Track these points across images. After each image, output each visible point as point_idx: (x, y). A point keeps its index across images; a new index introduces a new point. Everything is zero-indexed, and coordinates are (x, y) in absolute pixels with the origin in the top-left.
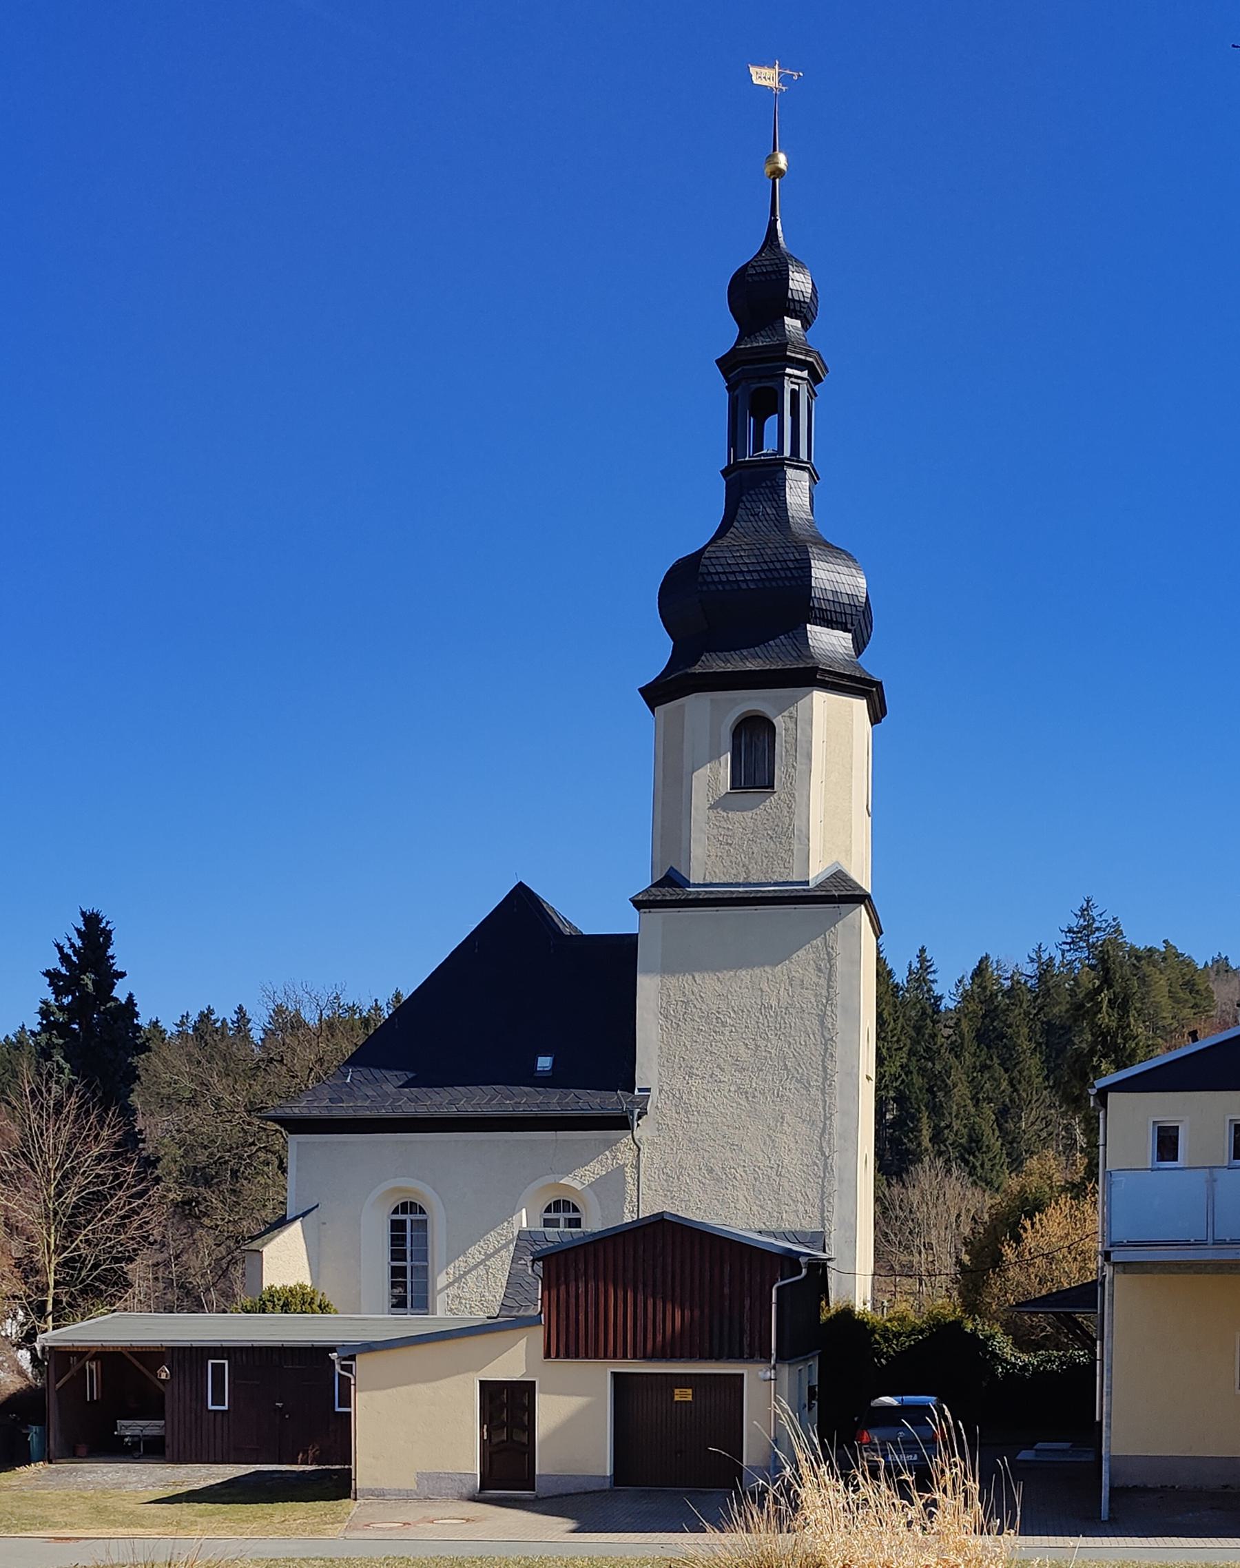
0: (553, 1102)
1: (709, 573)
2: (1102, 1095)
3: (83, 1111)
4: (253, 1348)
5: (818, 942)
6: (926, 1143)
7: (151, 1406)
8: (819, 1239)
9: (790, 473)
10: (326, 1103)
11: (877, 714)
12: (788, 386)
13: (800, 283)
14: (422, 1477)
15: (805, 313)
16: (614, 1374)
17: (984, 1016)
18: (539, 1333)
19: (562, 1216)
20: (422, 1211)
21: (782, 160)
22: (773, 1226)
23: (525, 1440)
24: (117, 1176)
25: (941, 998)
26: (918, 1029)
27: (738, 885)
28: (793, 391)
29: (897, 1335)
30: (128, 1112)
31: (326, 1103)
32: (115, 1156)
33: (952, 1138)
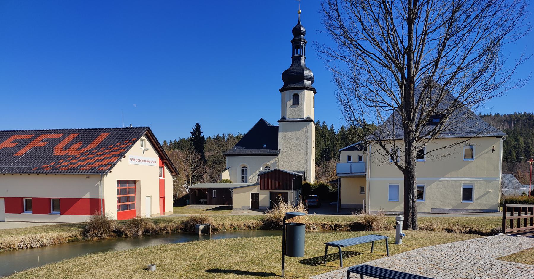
0: (266, 151)
1: (289, 73)
2: (340, 151)
3: (195, 154)
4: (224, 188)
5: (306, 127)
6: (332, 156)
7: (205, 197)
8: (303, 172)
9: (301, 58)
10: (232, 152)
11: (315, 93)
12: (301, 45)
13: (303, 29)
14: (243, 207)
15: (304, 34)
16: (270, 192)
17: (343, 135)
18: (259, 186)
19: (267, 168)
20: (246, 168)
21: (300, 11)
22: (296, 170)
23: (257, 201)
24: (200, 163)
25: (335, 132)
26: (332, 137)
27: (293, 119)
28: (302, 45)
29: (315, 186)
30: (202, 153)
31: (232, 152)
32: (200, 160)
33: (337, 155)
